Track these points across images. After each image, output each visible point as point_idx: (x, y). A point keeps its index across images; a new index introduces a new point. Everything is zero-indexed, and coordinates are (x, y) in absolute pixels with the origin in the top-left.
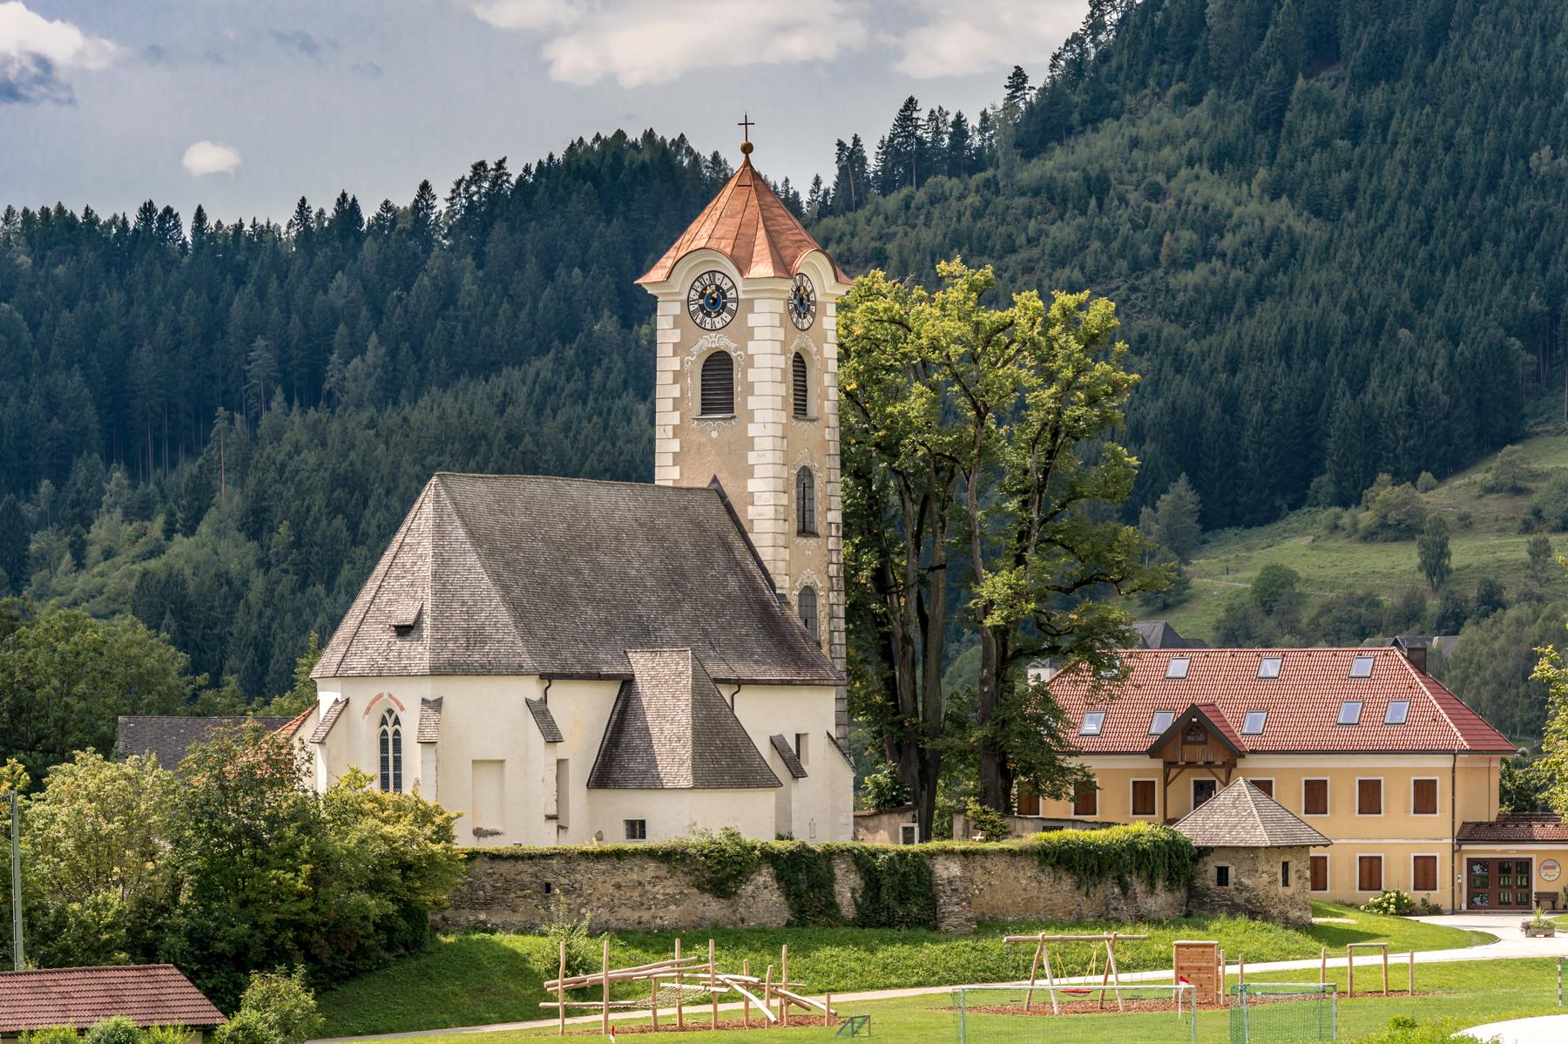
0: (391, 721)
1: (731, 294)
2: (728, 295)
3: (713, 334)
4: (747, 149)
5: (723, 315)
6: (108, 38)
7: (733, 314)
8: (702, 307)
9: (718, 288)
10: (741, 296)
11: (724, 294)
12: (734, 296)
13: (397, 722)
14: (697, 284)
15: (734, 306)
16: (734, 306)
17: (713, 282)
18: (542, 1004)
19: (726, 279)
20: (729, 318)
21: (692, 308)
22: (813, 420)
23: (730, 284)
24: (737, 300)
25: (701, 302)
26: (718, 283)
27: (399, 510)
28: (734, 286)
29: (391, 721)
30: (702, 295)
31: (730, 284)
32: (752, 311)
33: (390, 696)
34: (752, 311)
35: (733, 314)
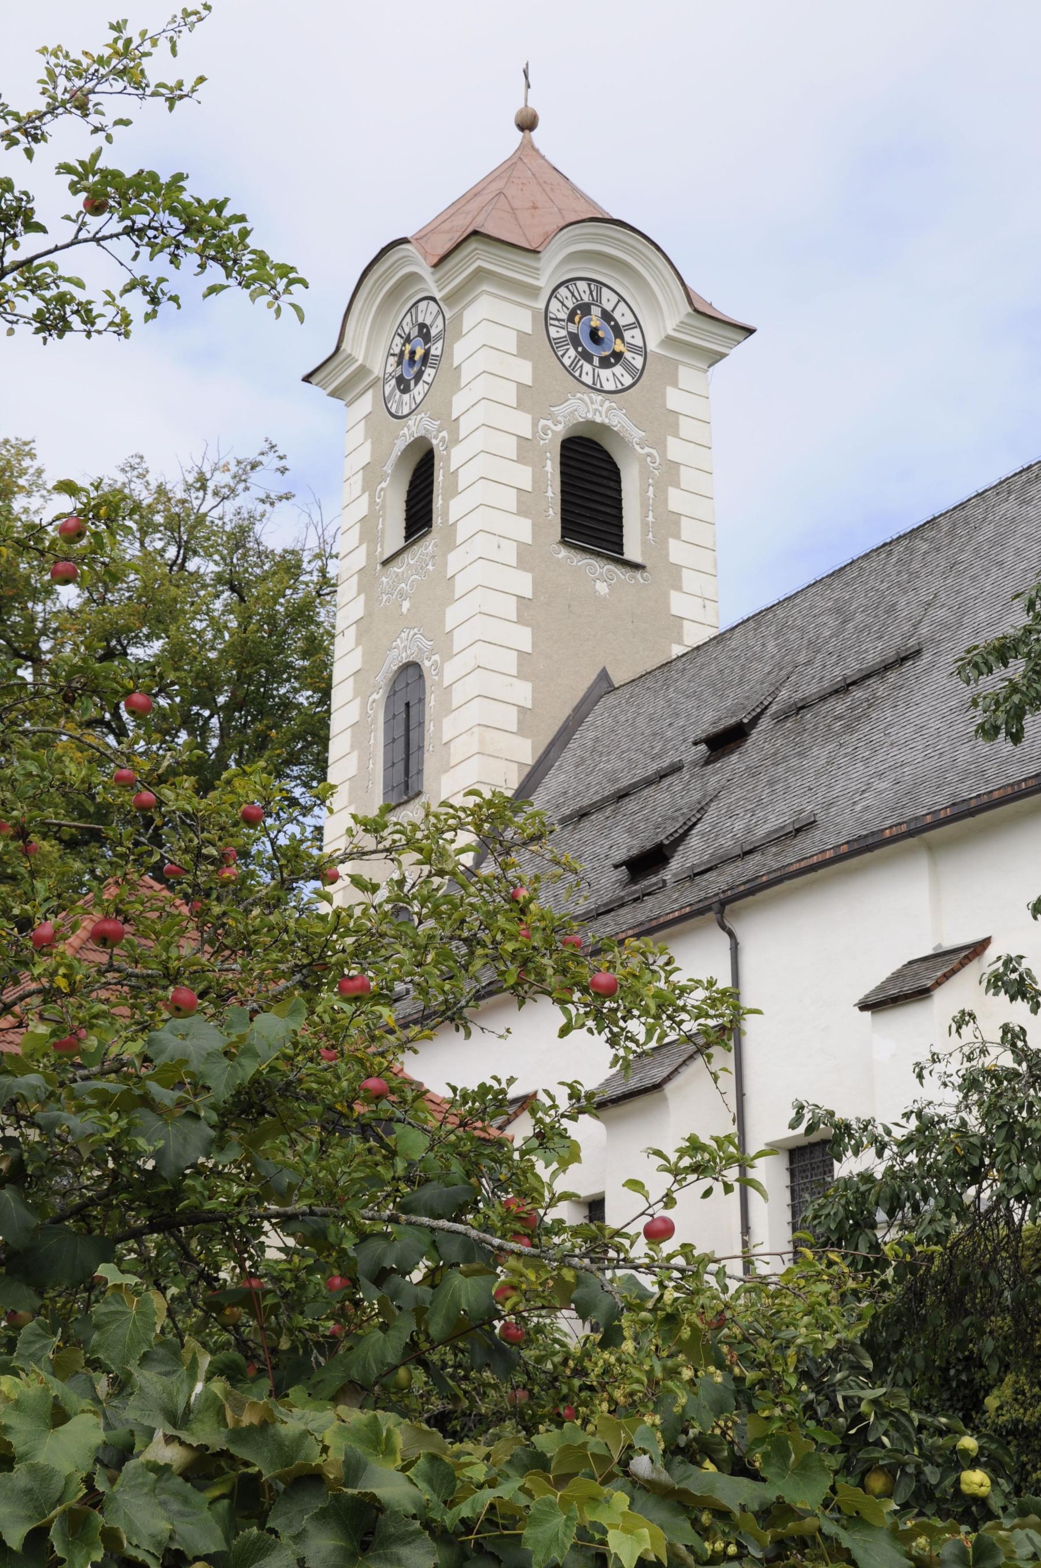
3: (598, 398)
4: (527, 124)
5: (618, 369)
7: (638, 376)
20: (628, 380)
24: (643, 351)
26: (609, 307)
28: (637, 324)
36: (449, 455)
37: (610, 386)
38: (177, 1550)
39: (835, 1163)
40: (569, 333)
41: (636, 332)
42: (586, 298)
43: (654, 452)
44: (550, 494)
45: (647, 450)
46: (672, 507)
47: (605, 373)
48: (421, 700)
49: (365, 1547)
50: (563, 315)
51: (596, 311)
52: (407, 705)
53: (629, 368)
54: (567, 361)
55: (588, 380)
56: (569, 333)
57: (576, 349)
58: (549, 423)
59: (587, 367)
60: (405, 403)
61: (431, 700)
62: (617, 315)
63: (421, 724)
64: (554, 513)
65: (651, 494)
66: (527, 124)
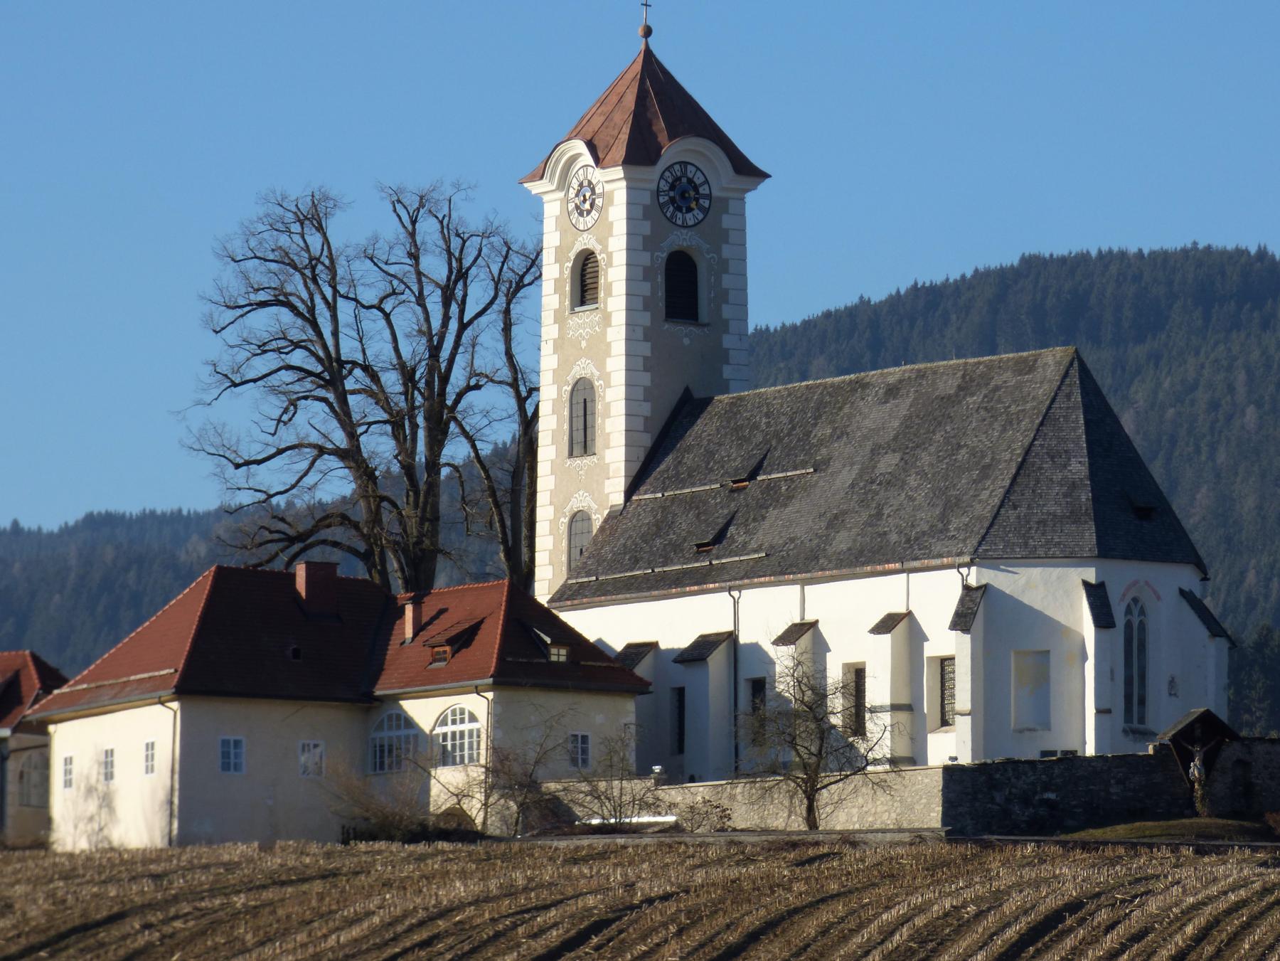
0: (1136, 612)
1: (704, 190)
2: (701, 190)
3: (684, 231)
4: (648, 32)
6: (577, 933)
8: (672, 201)
9: (690, 181)
10: (715, 193)
11: (696, 188)
12: (707, 192)
13: (1142, 612)
14: (667, 174)
15: (706, 203)
16: (706, 203)
17: (684, 174)
18: (582, 663)
19: (699, 173)
20: (700, 216)
21: (662, 200)
22: (707, 325)
23: (702, 179)
24: (709, 197)
25: (672, 194)
26: (690, 175)
27: (403, 405)
28: (706, 182)
29: (1136, 612)
30: (672, 187)
31: (693, 169)
32: (727, 212)
33: (1147, 583)
34: (727, 212)
35: (706, 211)
36: (605, 394)
37: (690, 223)
38: (555, 800)
39: (779, 328)
40: (670, 197)
41: (706, 187)
42: (679, 174)
43: (715, 255)
44: (660, 294)
45: (711, 255)
46: (649, 344)
47: (689, 216)
48: (593, 401)
49: (583, 303)
50: (667, 188)
51: (684, 180)
52: (585, 400)
53: (701, 208)
54: (668, 214)
55: (679, 222)
56: (670, 197)
57: (673, 205)
58: (659, 253)
59: (679, 215)
60: (583, 223)
61: (599, 406)
62: (695, 180)
63: (593, 440)
64: (662, 305)
65: (713, 280)
66: (648, 32)
